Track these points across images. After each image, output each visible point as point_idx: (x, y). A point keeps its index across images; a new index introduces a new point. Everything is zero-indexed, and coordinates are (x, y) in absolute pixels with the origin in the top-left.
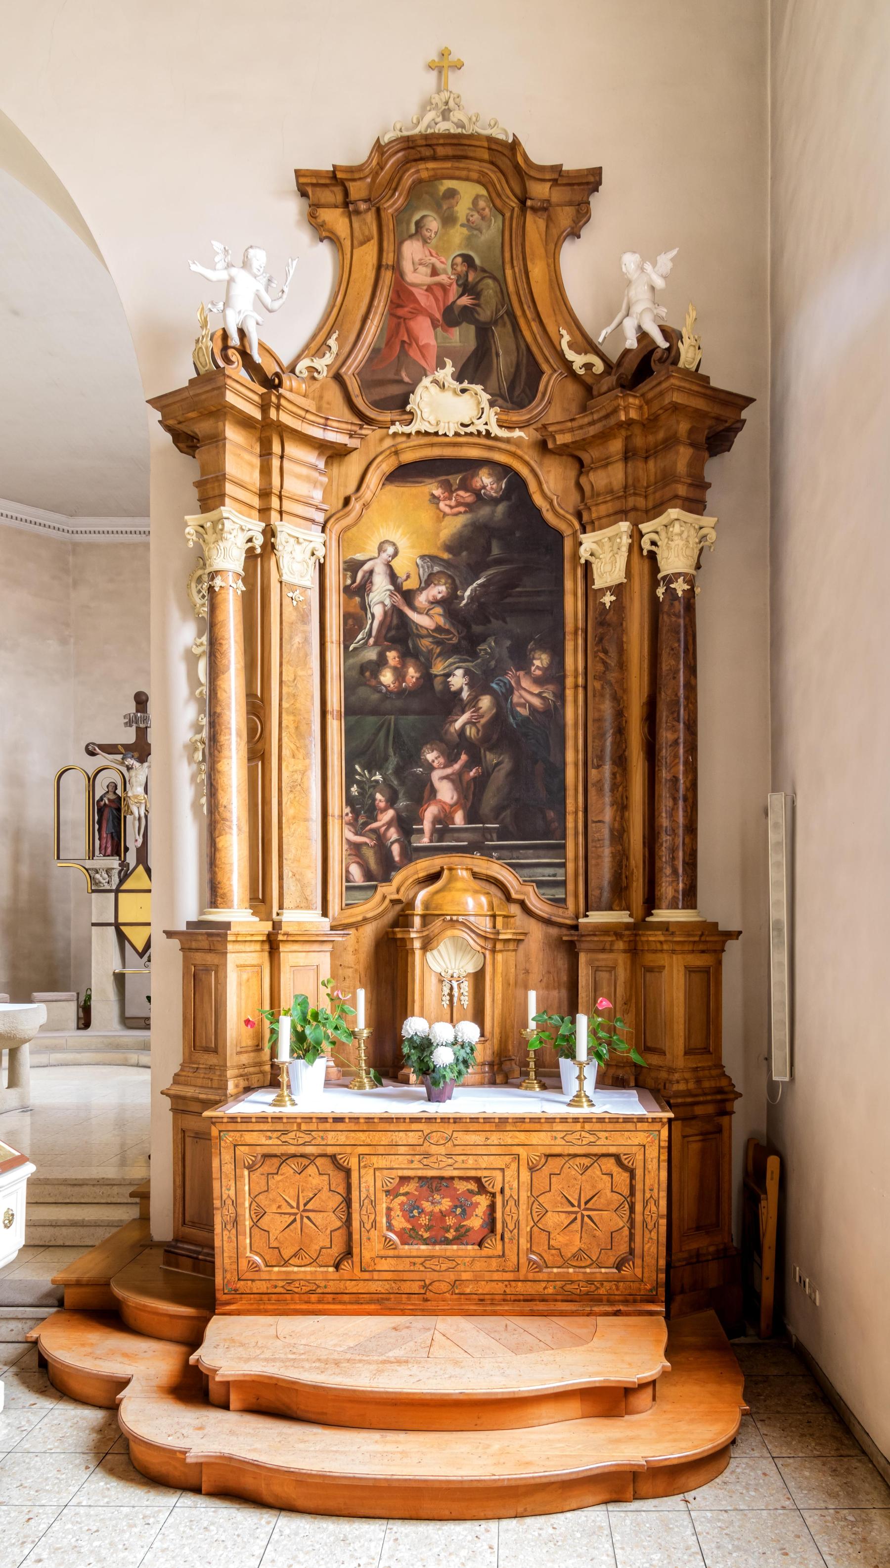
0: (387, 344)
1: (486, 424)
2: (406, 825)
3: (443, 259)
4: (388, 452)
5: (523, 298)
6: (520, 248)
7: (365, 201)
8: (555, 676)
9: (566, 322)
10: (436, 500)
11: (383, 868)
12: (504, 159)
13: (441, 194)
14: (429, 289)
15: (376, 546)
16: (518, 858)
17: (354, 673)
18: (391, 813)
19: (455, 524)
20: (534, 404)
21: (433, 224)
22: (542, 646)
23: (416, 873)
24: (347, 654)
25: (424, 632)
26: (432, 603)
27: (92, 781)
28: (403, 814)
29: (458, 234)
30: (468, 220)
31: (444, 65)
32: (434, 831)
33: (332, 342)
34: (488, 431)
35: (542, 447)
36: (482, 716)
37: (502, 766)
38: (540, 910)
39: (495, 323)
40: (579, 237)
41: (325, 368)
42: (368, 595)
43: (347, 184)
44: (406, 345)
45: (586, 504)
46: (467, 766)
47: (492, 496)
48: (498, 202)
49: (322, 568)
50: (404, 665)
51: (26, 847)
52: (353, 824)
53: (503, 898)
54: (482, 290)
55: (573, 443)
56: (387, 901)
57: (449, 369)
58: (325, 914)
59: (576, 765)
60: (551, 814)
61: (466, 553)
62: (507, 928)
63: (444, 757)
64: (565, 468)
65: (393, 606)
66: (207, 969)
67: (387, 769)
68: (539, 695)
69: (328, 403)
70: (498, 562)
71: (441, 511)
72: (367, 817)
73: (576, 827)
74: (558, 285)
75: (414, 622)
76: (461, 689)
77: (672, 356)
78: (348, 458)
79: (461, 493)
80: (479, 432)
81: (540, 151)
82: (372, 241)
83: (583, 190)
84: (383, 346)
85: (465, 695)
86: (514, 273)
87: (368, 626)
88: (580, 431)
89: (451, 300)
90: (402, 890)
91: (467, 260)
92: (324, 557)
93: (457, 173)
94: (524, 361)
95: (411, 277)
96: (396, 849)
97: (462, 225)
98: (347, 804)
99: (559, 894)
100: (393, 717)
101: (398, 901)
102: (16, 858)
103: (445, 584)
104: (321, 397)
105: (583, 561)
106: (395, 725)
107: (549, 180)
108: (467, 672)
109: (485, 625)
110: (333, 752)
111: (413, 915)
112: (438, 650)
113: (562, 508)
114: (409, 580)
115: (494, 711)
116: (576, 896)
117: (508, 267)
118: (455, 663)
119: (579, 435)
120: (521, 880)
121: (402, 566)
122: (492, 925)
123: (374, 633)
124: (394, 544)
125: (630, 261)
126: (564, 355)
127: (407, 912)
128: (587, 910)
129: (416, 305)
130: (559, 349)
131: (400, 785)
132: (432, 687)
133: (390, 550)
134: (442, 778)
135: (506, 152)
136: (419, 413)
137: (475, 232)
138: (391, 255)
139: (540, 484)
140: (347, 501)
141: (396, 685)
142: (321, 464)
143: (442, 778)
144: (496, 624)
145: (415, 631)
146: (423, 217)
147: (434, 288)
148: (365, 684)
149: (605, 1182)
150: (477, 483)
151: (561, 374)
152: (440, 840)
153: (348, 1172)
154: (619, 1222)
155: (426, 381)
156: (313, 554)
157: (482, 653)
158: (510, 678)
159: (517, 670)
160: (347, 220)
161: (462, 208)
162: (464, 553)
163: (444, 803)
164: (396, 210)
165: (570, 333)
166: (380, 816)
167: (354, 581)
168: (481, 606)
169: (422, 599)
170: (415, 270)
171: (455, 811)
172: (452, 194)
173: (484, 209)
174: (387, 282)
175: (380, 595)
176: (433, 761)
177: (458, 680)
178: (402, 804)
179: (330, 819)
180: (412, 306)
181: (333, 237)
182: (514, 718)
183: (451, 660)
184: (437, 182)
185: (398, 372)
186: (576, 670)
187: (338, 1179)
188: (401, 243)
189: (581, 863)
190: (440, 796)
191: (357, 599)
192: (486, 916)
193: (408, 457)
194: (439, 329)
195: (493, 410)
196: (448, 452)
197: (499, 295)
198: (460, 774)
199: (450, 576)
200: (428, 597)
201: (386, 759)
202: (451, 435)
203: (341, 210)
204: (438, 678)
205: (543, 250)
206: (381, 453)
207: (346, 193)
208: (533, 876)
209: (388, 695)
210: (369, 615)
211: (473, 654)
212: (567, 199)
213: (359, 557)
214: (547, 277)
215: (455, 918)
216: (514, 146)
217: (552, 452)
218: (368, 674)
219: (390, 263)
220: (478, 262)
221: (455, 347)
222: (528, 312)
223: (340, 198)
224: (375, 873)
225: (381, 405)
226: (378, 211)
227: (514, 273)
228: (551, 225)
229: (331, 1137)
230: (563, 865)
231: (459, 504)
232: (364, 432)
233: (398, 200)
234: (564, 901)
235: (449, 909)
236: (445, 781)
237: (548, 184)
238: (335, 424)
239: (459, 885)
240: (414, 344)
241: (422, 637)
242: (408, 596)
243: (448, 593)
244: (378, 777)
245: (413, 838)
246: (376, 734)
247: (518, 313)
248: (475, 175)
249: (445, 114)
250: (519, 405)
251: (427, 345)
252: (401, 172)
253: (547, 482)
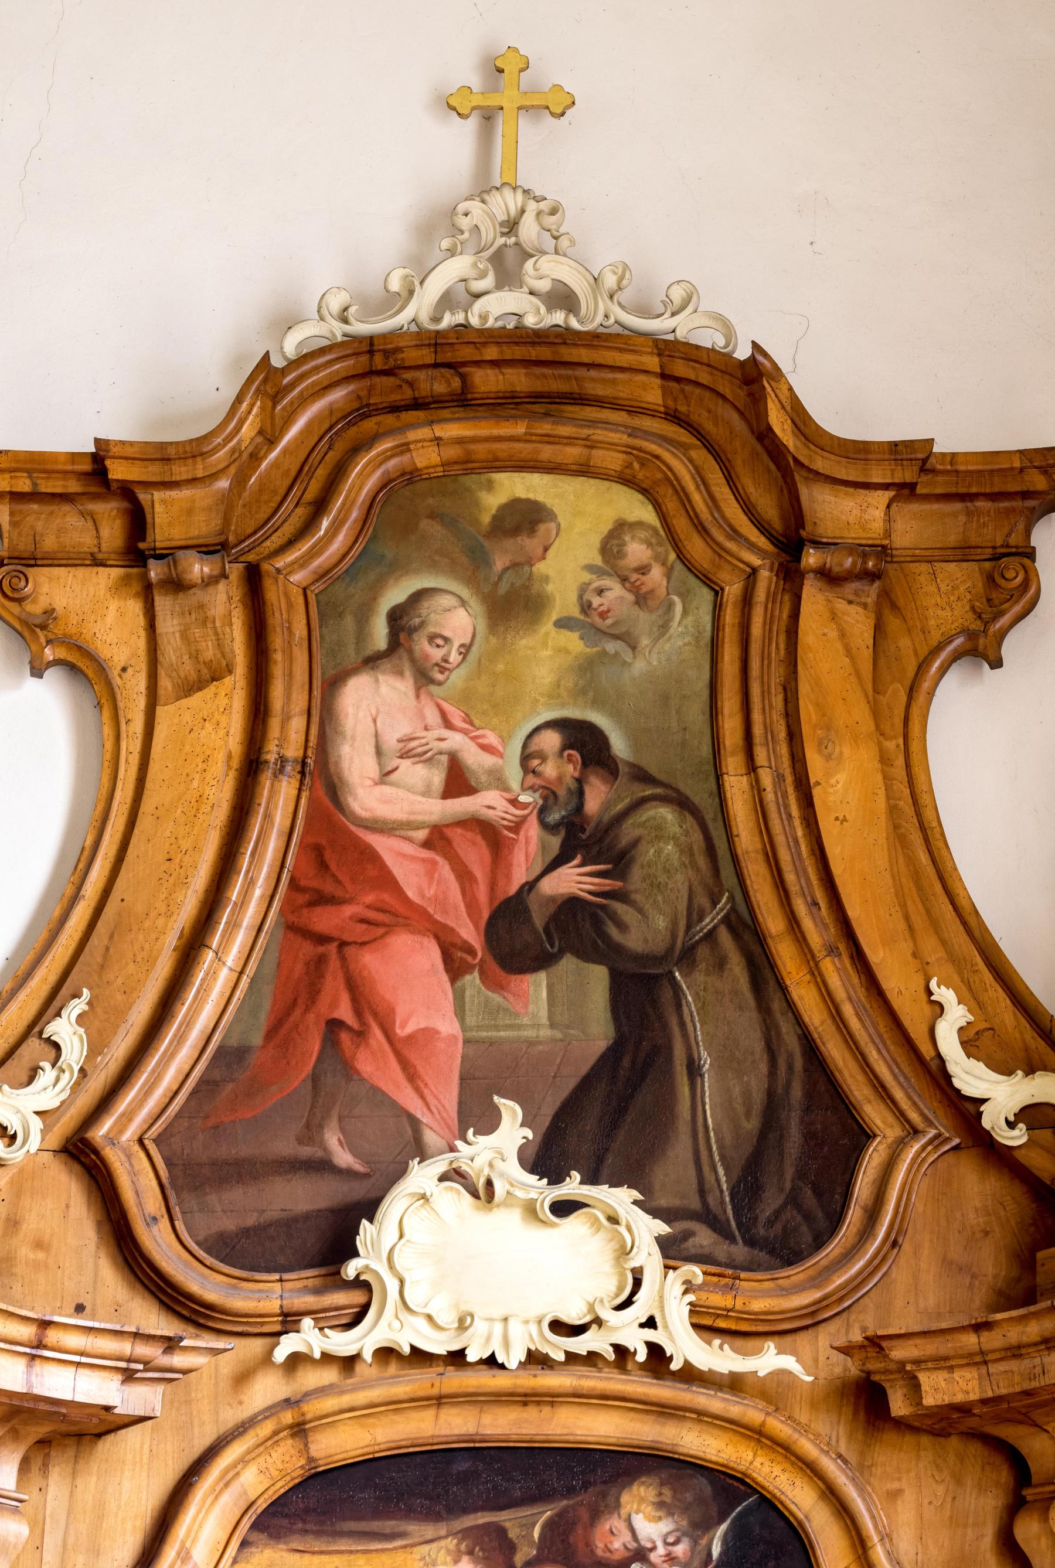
0: (270, 1034)
1: (650, 1323)
3: (492, 739)
4: (267, 1428)
5: (790, 877)
6: (778, 701)
7: (207, 550)
9: (954, 959)
12: (725, 402)
13: (486, 519)
14: (438, 838)
20: (833, 1248)
29: (546, 656)
30: (586, 607)
31: (500, 98)
33: (64, 1028)
34: (655, 1350)
35: (866, 1400)
39: (687, 957)
40: (996, 663)
43: (143, 496)
44: (344, 1037)
48: (697, 548)
54: (636, 843)
55: (984, 1402)
64: (959, 1481)
69: (39, 1245)
74: (922, 828)
80: (622, 1352)
82: (228, 680)
83: (1009, 512)
84: (257, 1039)
86: (757, 788)
88: (1013, 1365)
89: (520, 876)
91: (584, 741)
93: (547, 452)
94: (797, 1092)
95: (367, 797)
97: (563, 624)
107: (886, 487)
117: (733, 763)
126: (948, 1077)
129: (386, 897)
130: (927, 1052)
135: (725, 387)
136: (392, 1286)
137: (611, 646)
138: (297, 724)
146: (418, 596)
147: (457, 835)
151: (938, 1140)
155: (422, 1176)
160: (134, 608)
161: (565, 567)
164: (322, 575)
165: (970, 996)
170: (385, 776)
172: (525, 519)
173: (643, 570)
174: (280, 819)
180: (370, 898)
181: (81, 664)
184: (470, 481)
185: (311, 1132)
188: (334, 683)
193: (342, 1443)
194: (472, 980)
195: (675, 1281)
196: (502, 1425)
197: (702, 861)
202: (512, 1364)
203: (116, 572)
205: (860, 713)
207: (137, 521)
212: (952, 540)
214: (881, 804)
219: (293, 751)
220: (619, 745)
221: (531, 1043)
222: (808, 924)
223: (112, 531)
225: (240, 1251)
226: (254, 580)
227: (757, 788)
228: (893, 623)
232: (178, 1360)
233: (334, 538)
237: (882, 498)
240: (377, 1032)
247: (773, 923)
248: (614, 461)
249: (507, 266)
250: (783, 1252)
251: (429, 1034)
252: (340, 447)
253: (886, 1537)
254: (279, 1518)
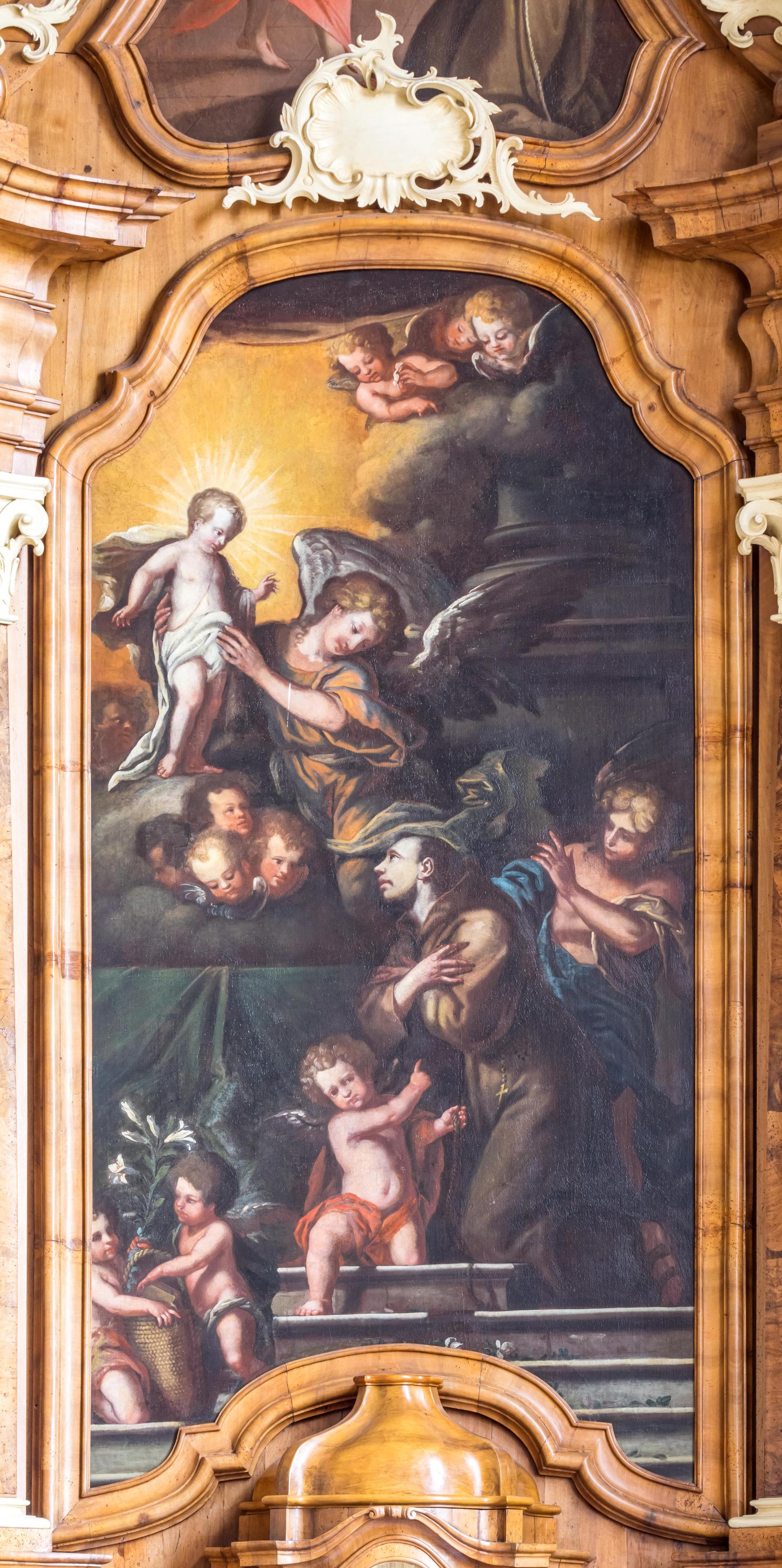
1: (486, 179)
2: (260, 1265)
4: (219, 256)
8: (670, 856)
10: (348, 382)
11: (206, 1382)
15: (184, 505)
16: (564, 1355)
17: (120, 851)
18: (216, 1234)
19: (400, 444)
20: (615, 124)
22: (635, 776)
23: (287, 1394)
24: (102, 796)
25: (314, 738)
26: (335, 659)
28: (252, 1236)
32: (335, 1281)
34: (490, 199)
35: (637, 235)
36: (469, 968)
37: (523, 1102)
38: (626, 1496)
41: (54, 33)
42: (160, 638)
45: (754, 396)
46: (428, 1105)
47: (499, 370)
49: (36, 567)
50: (256, 829)
52: (112, 1263)
53: (524, 1462)
55: (719, 236)
56: (206, 1474)
57: (390, 36)
58: (36, 1507)
59: (726, 1098)
60: (656, 1235)
61: (426, 528)
62: (535, 1540)
63: (363, 1079)
65: (230, 669)
67: (209, 1113)
68: (626, 909)
69: (58, 123)
70: (517, 547)
71: (361, 410)
72: (153, 1244)
73: (724, 1270)
75: (284, 711)
76: (412, 894)
78: (109, 268)
79: (417, 361)
80: (467, 200)
85: (423, 908)
87: (160, 723)
88: (740, 209)
90: (248, 1442)
92: (44, 540)
96: (230, 1332)
98: (96, 1210)
99: (677, 1451)
100: (225, 970)
101: (236, 1474)
103: (370, 608)
104: (39, 107)
105: (745, 549)
106: (231, 991)
108: (431, 848)
109: (474, 716)
110: (60, 1068)
111: (283, 1505)
112: (350, 788)
113: (690, 402)
114: (273, 597)
115: (503, 952)
116: (723, 1458)
118: (395, 822)
119: (736, 219)
120: (572, 1413)
121: (250, 561)
122: (494, 1531)
123: (175, 741)
124: (233, 501)
125: (140, 1230)
127: (267, 1499)
128: (752, 1493)
131: (242, 1156)
132: (333, 885)
133: (222, 516)
134: (360, 1137)
139: (631, 338)
140: (106, 387)
141: (236, 881)
142: (39, 290)
143: (360, 1137)
144: (509, 716)
145: (288, 736)
148: (149, 882)
150: (459, 335)
151: (689, 44)
152: (352, 1305)
155: (326, 71)
156: (16, 533)
157: (471, 794)
158: (546, 862)
159: (567, 840)
162: (424, 525)
163: (364, 1204)
166: (187, 1242)
167: (122, 601)
168: (471, 668)
169: (307, 649)
171: (394, 1228)
175: (193, 639)
176: (335, 1091)
177: (404, 869)
178: (247, 1207)
179: (53, 1250)
182: (556, 973)
183: (384, 815)
185: (247, 38)
186: (727, 841)
189: (737, 1367)
190: (350, 1186)
191: (131, 650)
192: (479, 1507)
193: (272, 266)
195: (503, 148)
198: (407, 1126)
199: (383, 587)
200: (323, 642)
201: (206, 1085)
202: (390, 209)
204: (350, 864)
206: (202, 257)
208: (605, 1404)
209: (211, 911)
210: (163, 693)
211: (448, 800)
213: (138, 534)
215: (397, 1511)
217: (662, 253)
218: (157, 853)
224: (173, 1396)
225: (198, 126)
230: (689, 1374)
231: (410, 391)
232: (157, 206)
234: (690, 1470)
235: (378, 1489)
236: (367, 1145)
238: (84, 192)
239: (407, 1425)
241: (306, 751)
242: (270, 641)
243: (379, 632)
244: (183, 1134)
245: (279, 1300)
246: (178, 1018)
250: (579, 127)
253: (649, 333)
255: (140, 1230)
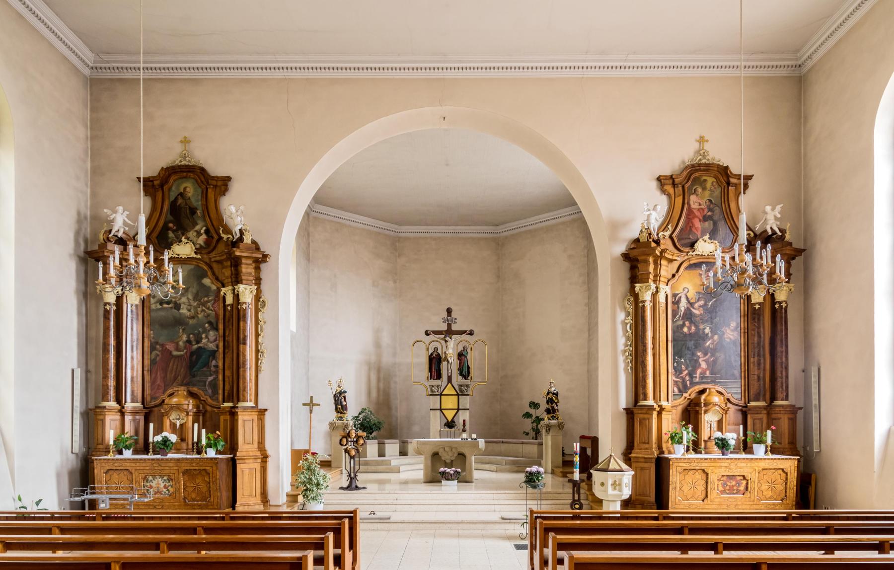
2: (691, 375)
12: (724, 171)
14: (699, 210)
21: (700, 190)
27: (427, 349)
29: (707, 193)
31: (702, 140)
51: (382, 376)
57: (708, 236)
66: (645, 419)
77: (782, 237)
81: (734, 169)
95: (693, 206)
96: (688, 383)
102: (379, 380)
121: (690, 295)
125: (768, 208)
149: (779, 477)
153: (707, 474)
154: (782, 488)
161: (709, 185)
169: (696, 305)
172: (705, 181)
177: (707, 330)
187: (704, 476)
193: (692, 262)
207: (674, 181)
216: (727, 168)
225: (685, 246)
229: (704, 464)
242: (692, 304)
254: (686, 268)
255: (768, 208)
